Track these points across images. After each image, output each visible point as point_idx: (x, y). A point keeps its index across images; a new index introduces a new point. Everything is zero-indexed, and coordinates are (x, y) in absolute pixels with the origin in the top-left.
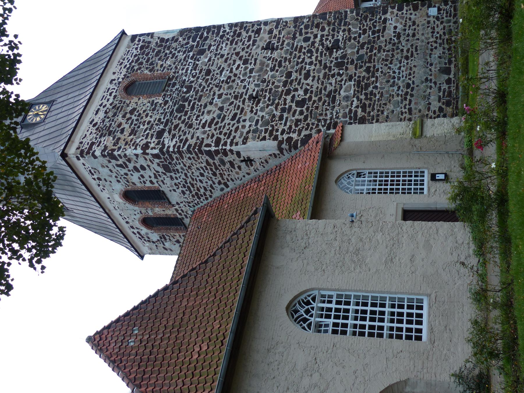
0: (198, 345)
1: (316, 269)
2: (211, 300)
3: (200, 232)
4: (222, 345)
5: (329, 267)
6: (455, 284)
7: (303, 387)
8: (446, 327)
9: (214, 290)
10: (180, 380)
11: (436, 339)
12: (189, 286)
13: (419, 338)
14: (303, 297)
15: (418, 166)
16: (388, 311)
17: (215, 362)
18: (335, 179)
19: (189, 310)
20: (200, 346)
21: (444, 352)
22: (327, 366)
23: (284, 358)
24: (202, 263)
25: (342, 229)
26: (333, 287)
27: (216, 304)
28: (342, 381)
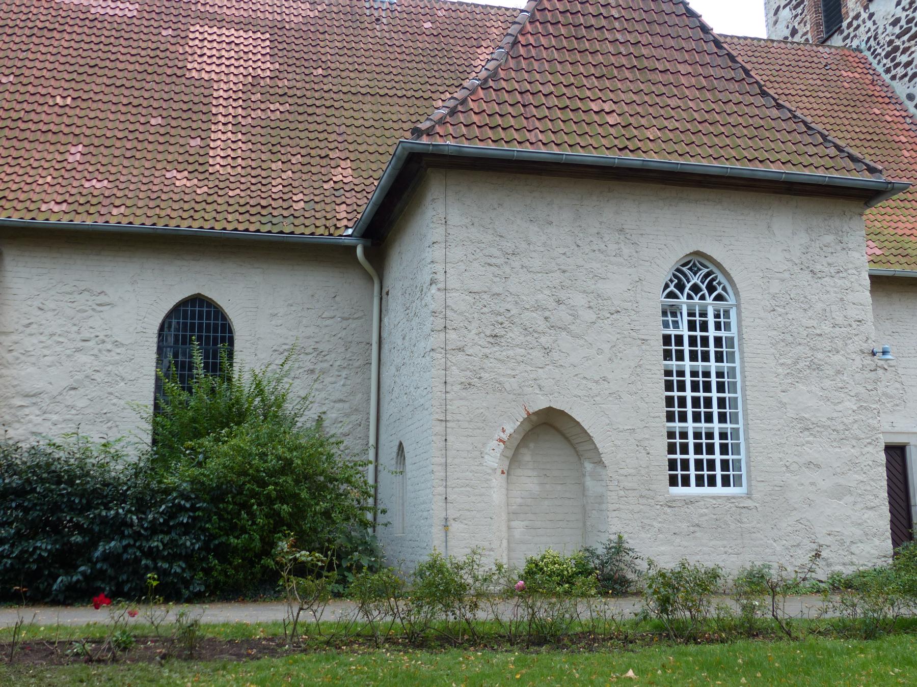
0: (614, 107)
1: (774, 297)
2: (696, 115)
3: (818, 71)
4: (620, 150)
5: (780, 318)
6: (775, 541)
7: (571, 296)
8: (698, 525)
9: (714, 117)
11: (676, 509)
12: (715, 72)
13: (673, 481)
14: (721, 278)
16: (713, 428)
17: (591, 141)
19: (671, 78)
20: (613, 111)
21: (655, 524)
22: (609, 333)
23: (613, 259)
24: (760, 87)
26: (744, 330)
27: (689, 126)
28: (587, 358)
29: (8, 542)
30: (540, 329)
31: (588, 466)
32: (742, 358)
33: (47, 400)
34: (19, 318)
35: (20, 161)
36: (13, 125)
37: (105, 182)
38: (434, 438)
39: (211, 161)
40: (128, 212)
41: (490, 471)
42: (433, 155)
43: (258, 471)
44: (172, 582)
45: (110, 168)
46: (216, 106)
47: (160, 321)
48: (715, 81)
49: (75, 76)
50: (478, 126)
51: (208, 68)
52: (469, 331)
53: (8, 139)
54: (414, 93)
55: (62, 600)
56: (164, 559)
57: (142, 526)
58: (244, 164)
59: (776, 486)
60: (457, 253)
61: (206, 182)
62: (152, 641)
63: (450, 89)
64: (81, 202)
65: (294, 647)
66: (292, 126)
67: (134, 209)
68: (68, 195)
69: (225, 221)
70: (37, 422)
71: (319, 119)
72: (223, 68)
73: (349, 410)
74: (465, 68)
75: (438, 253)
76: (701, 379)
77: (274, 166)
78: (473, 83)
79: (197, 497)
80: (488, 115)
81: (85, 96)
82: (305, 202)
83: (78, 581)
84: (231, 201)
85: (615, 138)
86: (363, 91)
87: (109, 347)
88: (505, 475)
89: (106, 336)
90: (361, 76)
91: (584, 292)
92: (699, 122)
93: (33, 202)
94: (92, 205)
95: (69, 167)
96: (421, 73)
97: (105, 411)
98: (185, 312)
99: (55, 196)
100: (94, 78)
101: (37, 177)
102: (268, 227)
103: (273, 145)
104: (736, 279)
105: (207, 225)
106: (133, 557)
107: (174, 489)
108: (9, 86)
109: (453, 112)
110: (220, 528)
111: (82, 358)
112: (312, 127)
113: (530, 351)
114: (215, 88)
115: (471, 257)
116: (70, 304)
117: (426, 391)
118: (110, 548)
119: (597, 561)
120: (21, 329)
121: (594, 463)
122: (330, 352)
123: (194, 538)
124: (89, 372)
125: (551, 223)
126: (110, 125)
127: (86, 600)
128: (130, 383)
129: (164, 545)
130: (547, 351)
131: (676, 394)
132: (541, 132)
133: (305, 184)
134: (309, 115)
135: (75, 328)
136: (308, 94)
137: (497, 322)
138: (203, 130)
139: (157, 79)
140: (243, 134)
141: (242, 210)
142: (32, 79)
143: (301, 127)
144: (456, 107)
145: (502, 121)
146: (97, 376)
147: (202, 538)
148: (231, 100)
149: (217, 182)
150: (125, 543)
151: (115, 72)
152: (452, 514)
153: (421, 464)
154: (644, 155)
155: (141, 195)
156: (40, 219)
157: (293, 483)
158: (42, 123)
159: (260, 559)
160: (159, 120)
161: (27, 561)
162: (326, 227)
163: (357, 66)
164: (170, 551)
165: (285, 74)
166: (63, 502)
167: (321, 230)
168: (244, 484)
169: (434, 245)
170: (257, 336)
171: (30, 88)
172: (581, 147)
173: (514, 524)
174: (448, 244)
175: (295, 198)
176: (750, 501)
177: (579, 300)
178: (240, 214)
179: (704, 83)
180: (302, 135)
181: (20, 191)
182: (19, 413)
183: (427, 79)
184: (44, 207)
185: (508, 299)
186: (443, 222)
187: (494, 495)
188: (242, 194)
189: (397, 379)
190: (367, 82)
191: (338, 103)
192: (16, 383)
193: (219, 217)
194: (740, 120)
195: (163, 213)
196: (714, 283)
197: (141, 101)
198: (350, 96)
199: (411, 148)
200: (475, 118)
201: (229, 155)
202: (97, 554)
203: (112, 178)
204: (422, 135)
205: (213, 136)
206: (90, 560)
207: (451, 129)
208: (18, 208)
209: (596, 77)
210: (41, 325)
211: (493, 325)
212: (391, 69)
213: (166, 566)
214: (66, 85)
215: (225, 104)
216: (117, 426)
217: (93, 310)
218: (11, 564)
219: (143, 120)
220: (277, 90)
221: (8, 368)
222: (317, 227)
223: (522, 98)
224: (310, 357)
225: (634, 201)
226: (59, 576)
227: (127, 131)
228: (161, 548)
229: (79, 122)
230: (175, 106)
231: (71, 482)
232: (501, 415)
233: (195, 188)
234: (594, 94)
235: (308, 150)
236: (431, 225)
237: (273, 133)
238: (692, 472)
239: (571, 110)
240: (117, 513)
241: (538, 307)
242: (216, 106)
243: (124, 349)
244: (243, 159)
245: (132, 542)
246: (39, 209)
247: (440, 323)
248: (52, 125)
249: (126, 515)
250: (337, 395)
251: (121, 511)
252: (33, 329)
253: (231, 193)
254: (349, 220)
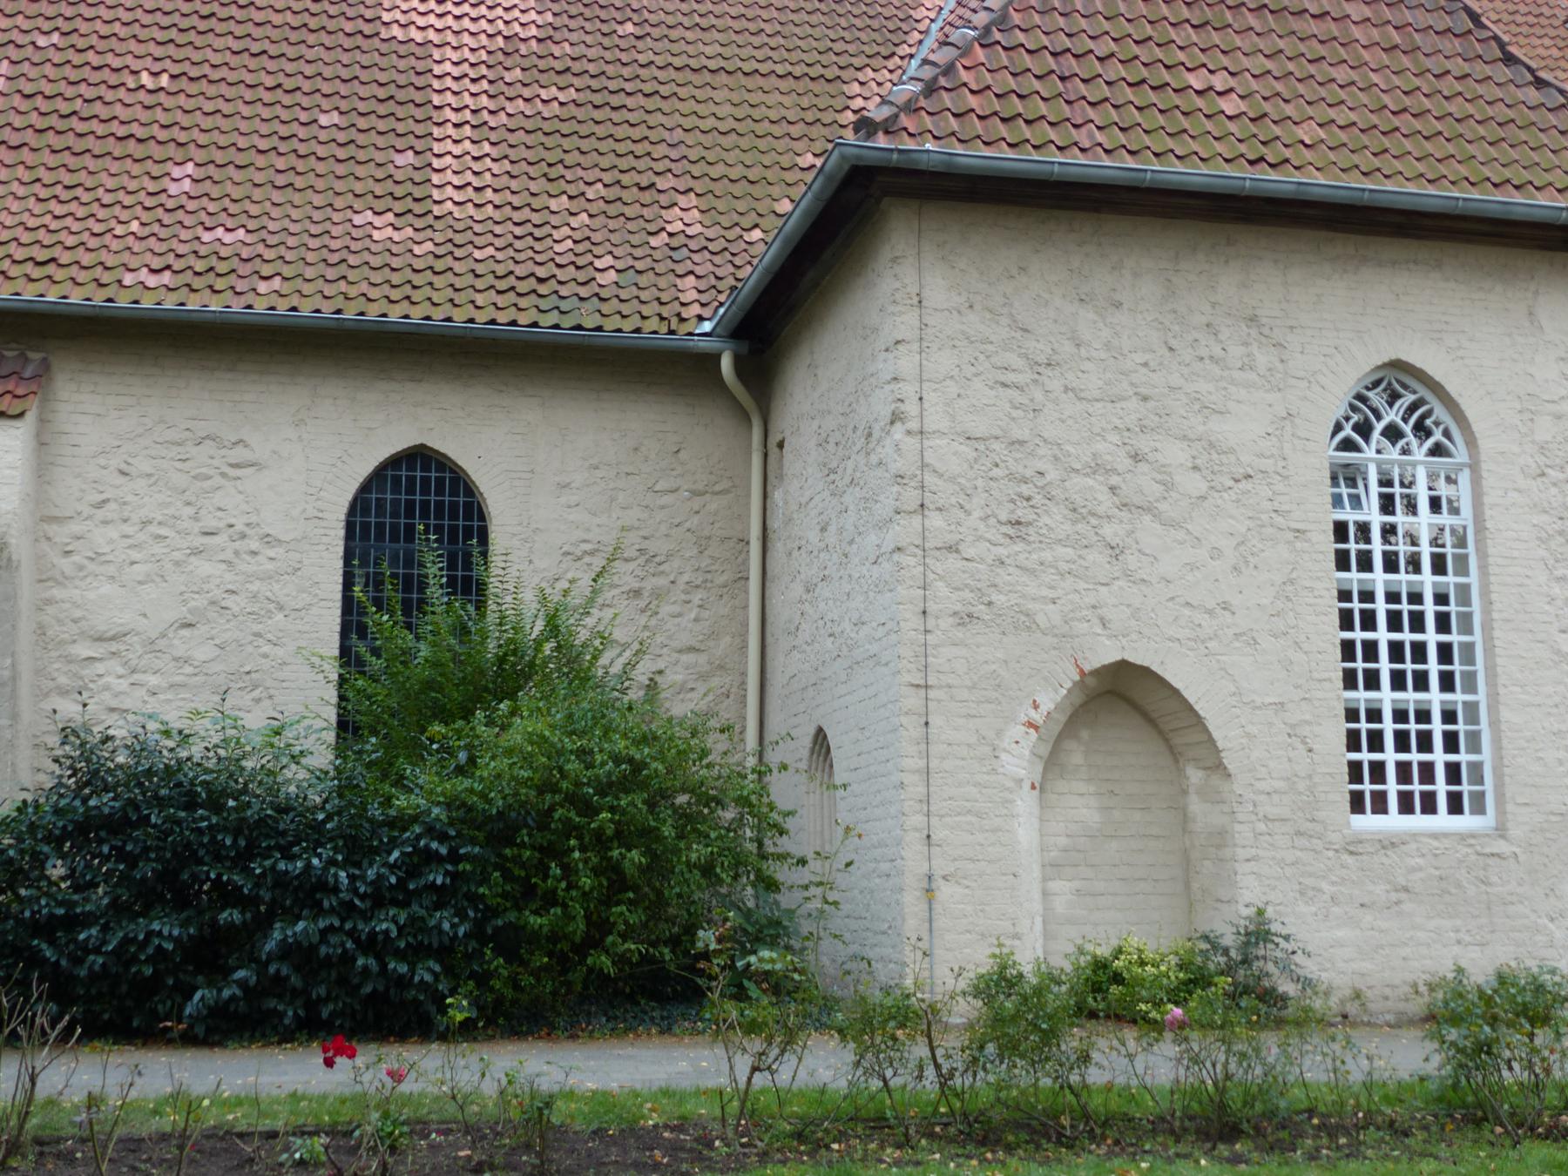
0: (1232, 82)
1: (1543, 449)
2: (1386, 99)
3: (1552, 32)
4: (1251, 163)
5: (1554, 491)
6: (1552, 920)
7: (1158, 445)
8: (1406, 890)
9: (1420, 103)
10: (1113, 46)
11: (1364, 857)
12: (1414, 18)
13: (1357, 804)
14: (1440, 412)
16: (1381, 701)
17: (1195, 146)
19: (1334, 29)
20: (1231, 90)
21: (1324, 886)
22: (1231, 517)
23: (1237, 374)
24: (1502, 45)
26: (1488, 513)
27: (1374, 119)
28: (1192, 567)
29: (95, 923)
30: (1101, 510)
31: (1195, 776)
32: (1483, 569)
33: (138, 647)
34: (83, 491)
35: (79, 192)
36: (61, 125)
37: (241, 233)
38: (904, 720)
39: (436, 195)
40: (286, 288)
41: (1010, 784)
42: (898, 171)
43: (578, 784)
44: (415, 1000)
45: (247, 205)
46: (439, 92)
47: (350, 497)
48: (1416, 35)
49: (173, 33)
50: (980, 117)
51: (421, 22)
52: (968, 513)
53: (54, 152)
54: (806, 70)
55: (201, 1036)
56: (401, 955)
57: (355, 891)
58: (497, 199)
59: (1553, 813)
60: (942, 361)
61: (429, 233)
62: (439, 1132)
63: (873, 62)
64: (198, 269)
65: (743, 1145)
66: (584, 130)
67: (298, 283)
68: (172, 255)
69: (471, 306)
70: (121, 688)
71: (633, 117)
72: (449, 20)
73: (707, 668)
74: (900, 24)
75: (906, 362)
76: (1405, 607)
77: (553, 204)
78: (965, 35)
79: (459, 835)
80: (997, 95)
81: (194, 73)
82: (618, 271)
83: (233, 998)
84: (480, 269)
85: (1240, 141)
86: (712, 65)
87: (254, 545)
88: (1036, 792)
89: (248, 525)
90: (707, 37)
91: (1185, 438)
92: (1394, 113)
93: (107, 268)
94: (218, 275)
95: (170, 204)
96: (817, 32)
97: (247, 668)
98: (396, 481)
99: (148, 258)
100: (210, 37)
101: (113, 223)
102: (553, 318)
103: (550, 165)
104: (1471, 413)
105: (438, 314)
106: (340, 951)
107: (415, 819)
108: (51, 53)
109: (931, 89)
110: (505, 896)
111: (203, 567)
112: (621, 132)
113: (1084, 552)
114: (437, 57)
115: (970, 370)
116: (179, 465)
117: (881, 631)
118: (295, 934)
119: (1222, 960)
120: (87, 511)
121: (1205, 769)
122: (669, 556)
123: (456, 915)
124: (217, 593)
125: (1118, 305)
126: (244, 126)
127: (247, 1035)
128: (293, 615)
129: (400, 929)
130: (1115, 551)
131: (1358, 635)
132: (1099, 128)
133: (615, 238)
134: (613, 109)
135: (190, 511)
136: (610, 70)
137: (1020, 495)
138: (417, 137)
139: (328, 41)
140: (493, 144)
141: (502, 285)
142: (94, 40)
143: (601, 131)
144: (935, 79)
145: (1024, 107)
146: (230, 601)
147: (471, 914)
148: (467, 81)
149: (450, 234)
150: (322, 924)
151: (249, 28)
152: (940, 866)
153: (872, 769)
154: (1296, 173)
155: (310, 257)
156: (123, 302)
157: (645, 808)
158: (116, 123)
159: (585, 957)
160: (335, 118)
161: (134, 959)
162: (662, 319)
163: (698, 19)
164: (410, 939)
165: (567, 34)
166: (202, 845)
167: (653, 324)
168: (552, 809)
169: (899, 347)
170: (534, 526)
171: (91, 56)
172: (1178, 157)
173: (1055, 886)
174: (925, 344)
175: (598, 264)
176: (1502, 842)
177: (1175, 454)
178: (499, 292)
179: (1397, 38)
180: (604, 146)
181: (81, 249)
182: (85, 672)
183: (830, 44)
184: (128, 279)
185: (1041, 452)
186: (916, 300)
187: (1021, 831)
188: (500, 256)
189: (807, 607)
190: (720, 49)
191: (667, 87)
192: (78, 614)
193: (458, 298)
194: (1470, 109)
195: (353, 291)
196: (1428, 422)
197: (299, 81)
198: (687, 75)
199: (858, 157)
200: (973, 101)
201: (469, 184)
202: (270, 946)
203: (252, 225)
204: (875, 133)
205: (437, 148)
206: (253, 959)
207: (928, 122)
208: (80, 280)
209: (1193, 26)
210: (125, 503)
211: (1013, 501)
212: (763, 26)
213: (403, 969)
214: (159, 52)
215: (455, 87)
216: (270, 697)
217: (223, 475)
218: (104, 964)
219: (304, 117)
220: (552, 62)
221: (65, 586)
222: (644, 318)
223: (1057, 63)
224: (632, 566)
225: (1276, 261)
226: (195, 989)
227: (275, 137)
228: (394, 934)
229: (185, 121)
230: (364, 91)
231: (215, 805)
232: (1030, 677)
233: (410, 244)
234: (1192, 57)
235: (616, 174)
236: (892, 308)
237: (549, 142)
238: (1392, 787)
239: (1152, 88)
240: (309, 866)
241: (1097, 467)
242: (439, 92)
243: (281, 550)
244: (495, 191)
245: (337, 923)
246: (119, 281)
247: (911, 497)
248: (135, 124)
249: (325, 869)
250: (685, 639)
251: (315, 861)
252: (111, 510)
253: (478, 254)
254: (703, 305)
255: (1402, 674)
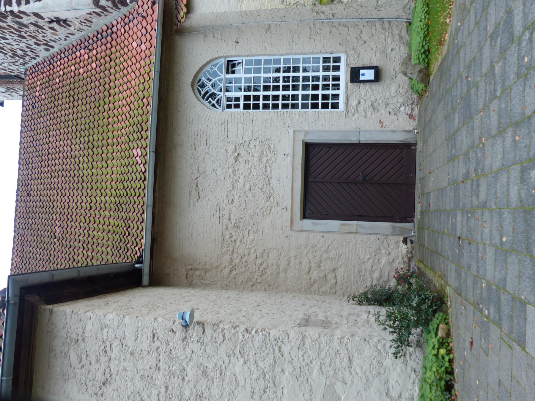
13: (335, 106)
15: (330, 50)
18: (190, 80)
25: (168, 344)
238: (330, 92)
255: (293, 86)
